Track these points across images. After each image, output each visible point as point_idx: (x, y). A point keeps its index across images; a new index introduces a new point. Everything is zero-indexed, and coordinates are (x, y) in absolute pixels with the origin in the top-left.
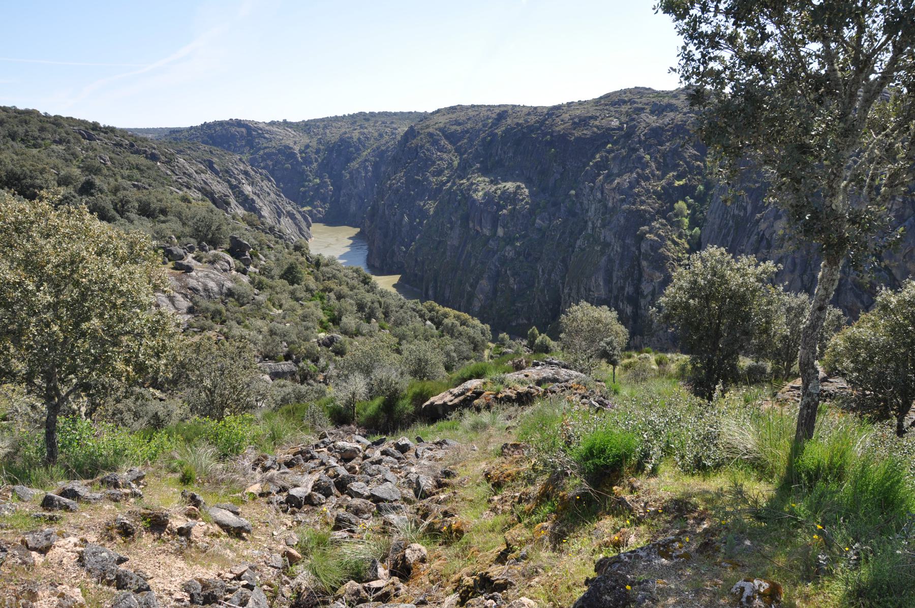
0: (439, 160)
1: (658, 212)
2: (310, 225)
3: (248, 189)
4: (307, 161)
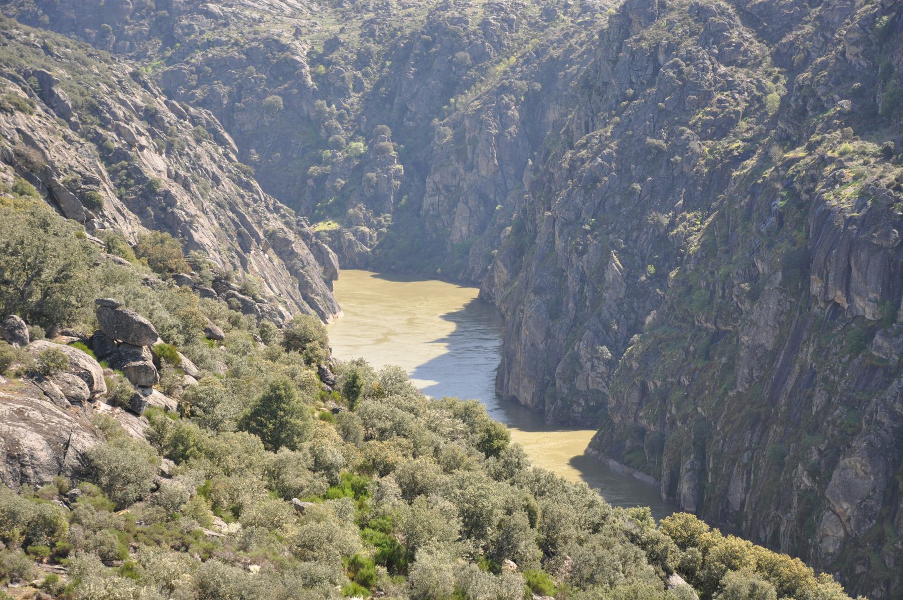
0: (722, 90)
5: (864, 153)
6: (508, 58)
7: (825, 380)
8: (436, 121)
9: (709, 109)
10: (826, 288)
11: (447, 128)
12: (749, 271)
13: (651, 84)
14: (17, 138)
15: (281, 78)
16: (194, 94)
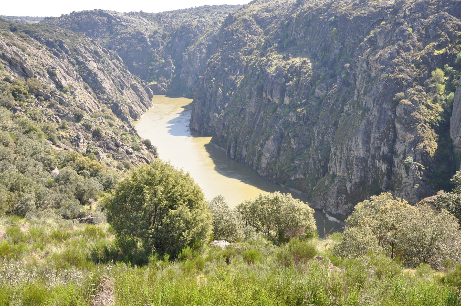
0: (250, 42)
1: (415, 80)
2: (152, 97)
3: (93, 66)
4: (155, 44)
5: (278, 58)
7: (266, 120)
8: (184, 53)
10: (266, 95)
13: (231, 40)
14: (13, 53)
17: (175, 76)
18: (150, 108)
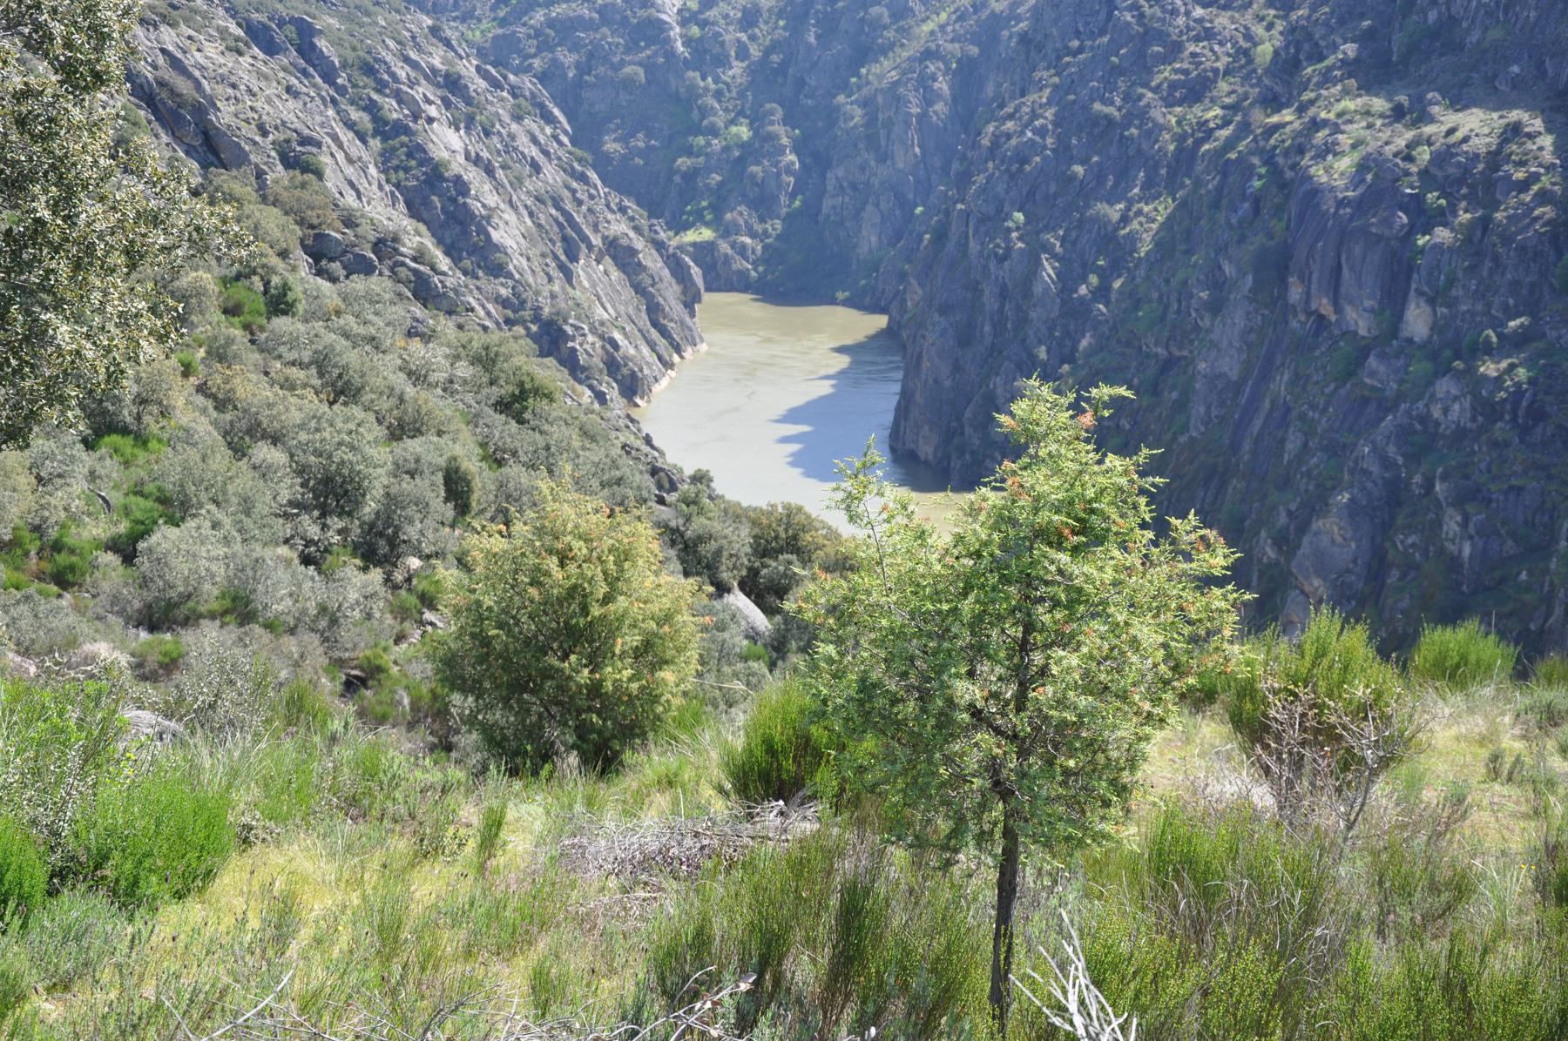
0: (1197, 39)
2: (697, 298)
4: (707, 55)
5: (1368, 113)
6: (938, 14)
7: (1302, 417)
9: (1178, 66)
10: (1308, 294)
11: (855, 107)
12: (1214, 276)
13: (1102, 32)
14: (161, 61)
15: (642, 44)
16: (530, 65)
17: (797, 203)
18: (689, 349)
